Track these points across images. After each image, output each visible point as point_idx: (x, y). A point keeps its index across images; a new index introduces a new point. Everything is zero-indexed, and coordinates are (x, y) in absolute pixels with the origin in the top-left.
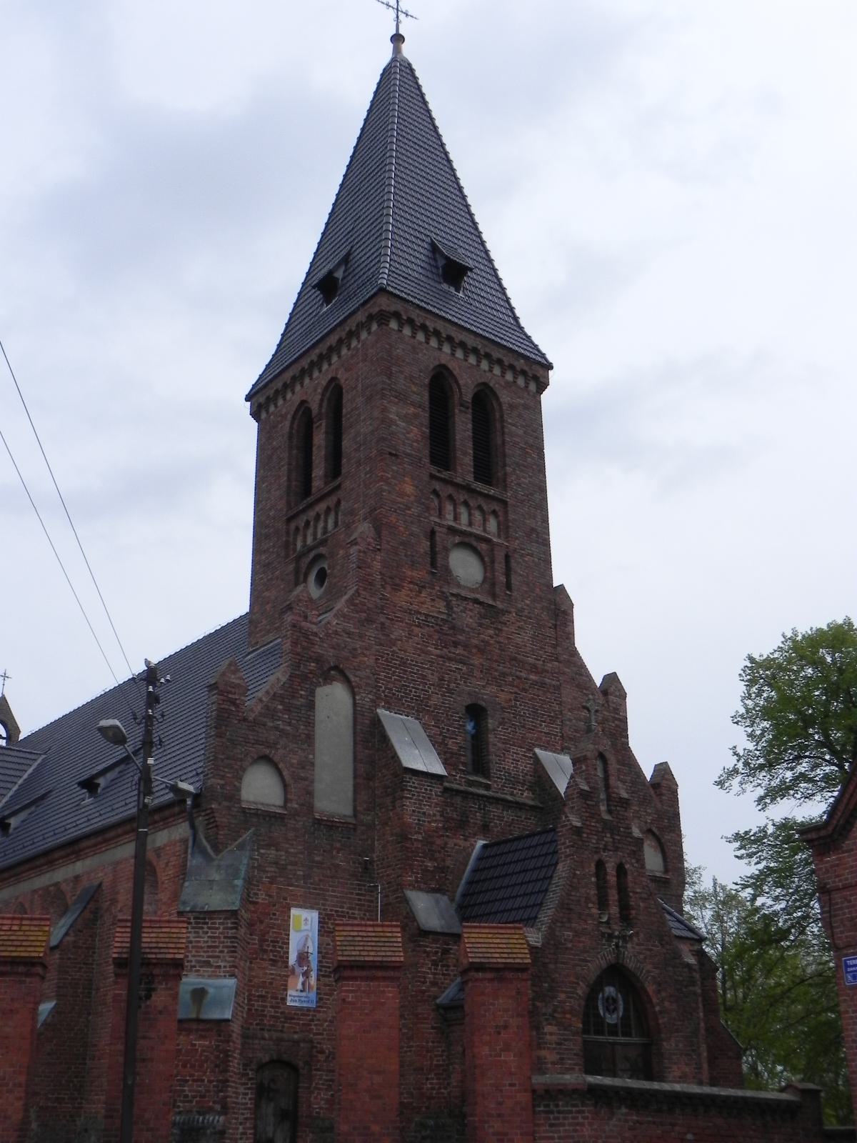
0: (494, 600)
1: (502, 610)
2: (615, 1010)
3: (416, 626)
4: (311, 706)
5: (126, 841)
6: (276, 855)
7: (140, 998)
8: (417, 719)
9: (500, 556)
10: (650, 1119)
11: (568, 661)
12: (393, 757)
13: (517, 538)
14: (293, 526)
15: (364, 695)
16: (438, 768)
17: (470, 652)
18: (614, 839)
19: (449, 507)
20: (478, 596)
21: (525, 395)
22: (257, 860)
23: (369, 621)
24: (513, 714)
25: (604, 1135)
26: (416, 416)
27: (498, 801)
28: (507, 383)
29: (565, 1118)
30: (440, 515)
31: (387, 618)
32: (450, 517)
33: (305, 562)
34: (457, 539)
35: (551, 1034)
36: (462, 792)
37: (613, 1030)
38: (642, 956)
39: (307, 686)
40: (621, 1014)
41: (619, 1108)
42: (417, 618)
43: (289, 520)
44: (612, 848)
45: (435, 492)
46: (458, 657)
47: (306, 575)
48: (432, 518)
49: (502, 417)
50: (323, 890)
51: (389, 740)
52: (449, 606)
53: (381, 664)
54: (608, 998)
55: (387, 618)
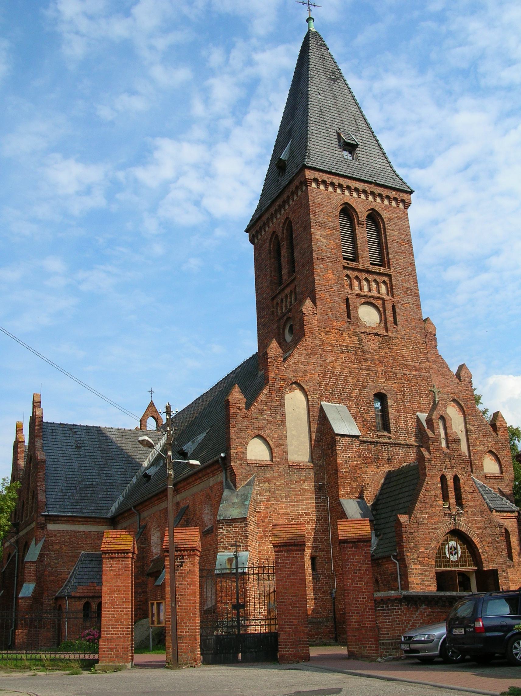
0: (387, 332)
1: (393, 337)
2: (457, 553)
3: (341, 353)
4: (283, 405)
5: (197, 483)
6: (269, 487)
7: (178, 566)
8: (344, 405)
9: (389, 306)
10: (439, 610)
11: (435, 361)
12: (330, 428)
13: (398, 295)
14: (275, 302)
15: (313, 395)
16: (356, 432)
17: (375, 364)
18: (451, 462)
19: (356, 283)
20: (377, 331)
21: (398, 211)
22: (259, 490)
23: (313, 354)
24: (403, 395)
25: (413, 620)
26: (331, 235)
27: (395, 445)
28: (386, 206)
29: (392, 612)
30: (351, 288)
31: (323, 351)
32: (357, 288)
33: (283, 321)
34: (363, 300)
35: (416, 569)
36: (374, 442)
37: (455, 564)
38: (470, 524)
39: (280, 395)
40: (459, 555)
41: (421, 606)
42: (341, 349)
43: (273, 299)
44: (450, 467)
45: (347, 276)
46: (368, 367)
47: (284, 330)
48: (346, 291)
49: (384, 226)
50: (296, 502)
51: (328, 419)
52: (360, 340)
53: (322, 377)
54: (451, 547)
55: (323, 351)
